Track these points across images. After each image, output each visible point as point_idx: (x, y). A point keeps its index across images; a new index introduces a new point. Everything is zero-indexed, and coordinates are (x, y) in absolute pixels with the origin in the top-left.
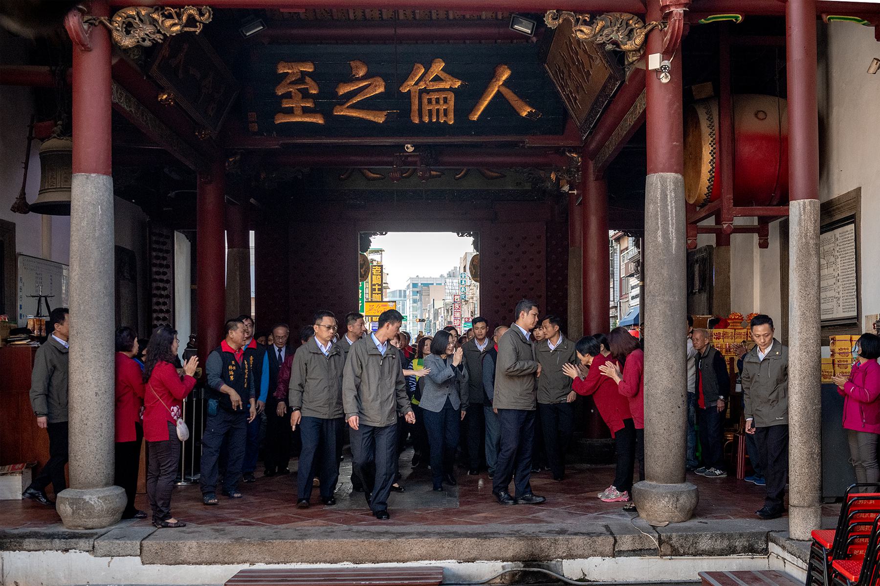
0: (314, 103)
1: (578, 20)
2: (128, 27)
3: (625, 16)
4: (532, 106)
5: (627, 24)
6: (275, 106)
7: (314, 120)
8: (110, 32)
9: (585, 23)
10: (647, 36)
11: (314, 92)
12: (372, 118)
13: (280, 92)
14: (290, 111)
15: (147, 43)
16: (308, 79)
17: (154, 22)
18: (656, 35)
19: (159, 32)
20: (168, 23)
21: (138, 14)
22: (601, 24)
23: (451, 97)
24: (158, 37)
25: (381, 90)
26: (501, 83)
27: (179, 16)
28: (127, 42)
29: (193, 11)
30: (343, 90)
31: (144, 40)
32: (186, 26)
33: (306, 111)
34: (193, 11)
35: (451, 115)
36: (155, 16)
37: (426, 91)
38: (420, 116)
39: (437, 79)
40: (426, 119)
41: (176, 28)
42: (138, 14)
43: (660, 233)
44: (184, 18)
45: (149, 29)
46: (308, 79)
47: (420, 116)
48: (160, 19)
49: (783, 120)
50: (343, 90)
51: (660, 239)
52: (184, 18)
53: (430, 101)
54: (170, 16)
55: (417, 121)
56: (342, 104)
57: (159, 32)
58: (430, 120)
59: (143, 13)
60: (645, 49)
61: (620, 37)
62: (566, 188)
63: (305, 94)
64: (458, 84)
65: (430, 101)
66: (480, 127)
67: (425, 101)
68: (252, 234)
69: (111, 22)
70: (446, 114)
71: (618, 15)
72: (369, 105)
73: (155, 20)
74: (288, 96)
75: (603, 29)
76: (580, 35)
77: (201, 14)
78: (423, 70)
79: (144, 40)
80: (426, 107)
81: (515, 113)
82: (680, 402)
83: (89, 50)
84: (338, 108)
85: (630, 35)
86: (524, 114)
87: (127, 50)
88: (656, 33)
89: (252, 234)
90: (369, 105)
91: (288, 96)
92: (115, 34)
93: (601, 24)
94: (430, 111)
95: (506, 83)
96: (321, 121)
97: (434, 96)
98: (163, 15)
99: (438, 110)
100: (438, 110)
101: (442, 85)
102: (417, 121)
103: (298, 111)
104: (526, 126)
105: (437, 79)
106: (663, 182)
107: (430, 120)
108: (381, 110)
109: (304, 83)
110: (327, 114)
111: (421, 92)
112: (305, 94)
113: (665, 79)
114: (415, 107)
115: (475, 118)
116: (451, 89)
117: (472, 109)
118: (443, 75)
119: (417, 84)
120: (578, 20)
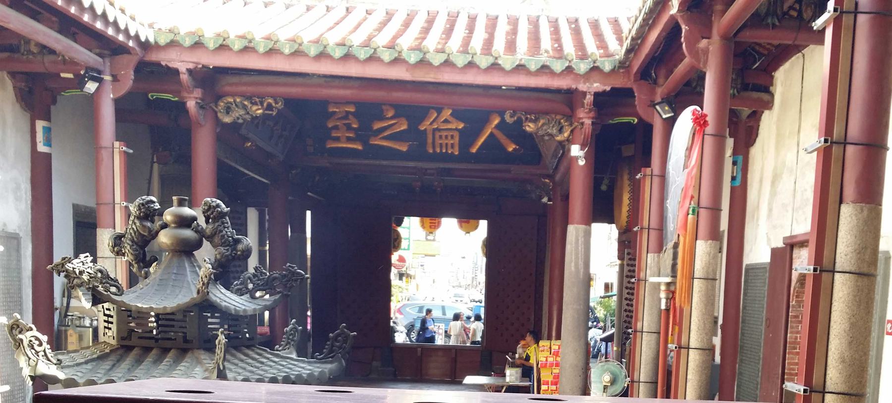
0: (356, 134)
1: (527, 118)
2: (228, 110)
3: (558, 117)
4: (516, 144)
5: (560, 123)
6: (327, 135)
7: (355, 146)
8: (216, 113)
9: (531, 121)
10: (572, 131)
11: (355, 126)
12: (398, 147)
13: (330, 125)
14: (337, 139)
15: (240, 121)
16: (350, 117)
17: (245, 107)
18: (577, 131)
19: (248, 113)
20: (255, 108)
21: (235, 101)
22: (542, 122)
23: (457, 135)
24: (248, 117)
25: (404, 127)
26: (493, 126)
27: (262, 103)
28: (227, 120)
29: (270, 101)
30: (377, 126)
31: (238, 118)
32: (266, 109)
33: (349, 140)
34: (270, 101)
35: (457, 148)
36: (246, 103)
37: (438, 129)
38: (434, 147)
39: (446, 121)
40: (438, 150)
41: (260, 112)
42: (235, 101)
43: (573, 264)
44: (265, 105)
45: (242, 112)
46: (350, 117)
47: (434, 147)
48: (250, 106)
49: (581, 248)
50: (377, 126)
51: (573, 269)
52: (265, 105)
53: (441, 137)
54: (255, 104)
55: (431, 151)
56: (376, 136)
57: (248, 113)
58: (441, 150)
59: (238, 100)
60: (570, 141)
61: (554, 131)
62: (545, 200)
63: (349, 128)
64: (461, 126)
65: (441, 137)
66: (476, 158)
67: (437, 136)
68: (309, 213)
69: (216, 106)
70: (452, 146)
71: (553, 116)
72: (397, 137)
73: (245, 105)
74: (336, 128)
75: (543, 125)
76: (528, 129)
77: (276, 103)
78: (436, 115)
79: (238, 118)
80: (438, 141)
81: (503, 149)
82: (581, 373)
83: (201, 126)
84: (373, 138)
85: (561, 131)
86: (510, 149)
87: (227, 124)
88: (577, 130)
89: (309, 213)
90: (397, 137)
91: (336, 128)
92: (219, 115)
93: (542, 122)
94: (441, 144)
95: (497, 127)
96: (360, 148)
97: (444, 134)
98: (252, 103)
99: (447, 144)
100: (447, 144)
101: (449, 126)
102: (431, 151)
103: (344, 139)
104: (510, 158)
105: (446, 121)
106: (577, 230)
107: (441, 150)
108: (406, 141)
109: (348, 119)
110: (365, 143)
111: (434, 130)
112: (349, 128)
113: (582, 162)
114: (430, 140)
115: (474, 150)
116: (456, 129)
117: (472, 144)
118: (451, 119)
119: (431, 124)
120: (527, 118)
